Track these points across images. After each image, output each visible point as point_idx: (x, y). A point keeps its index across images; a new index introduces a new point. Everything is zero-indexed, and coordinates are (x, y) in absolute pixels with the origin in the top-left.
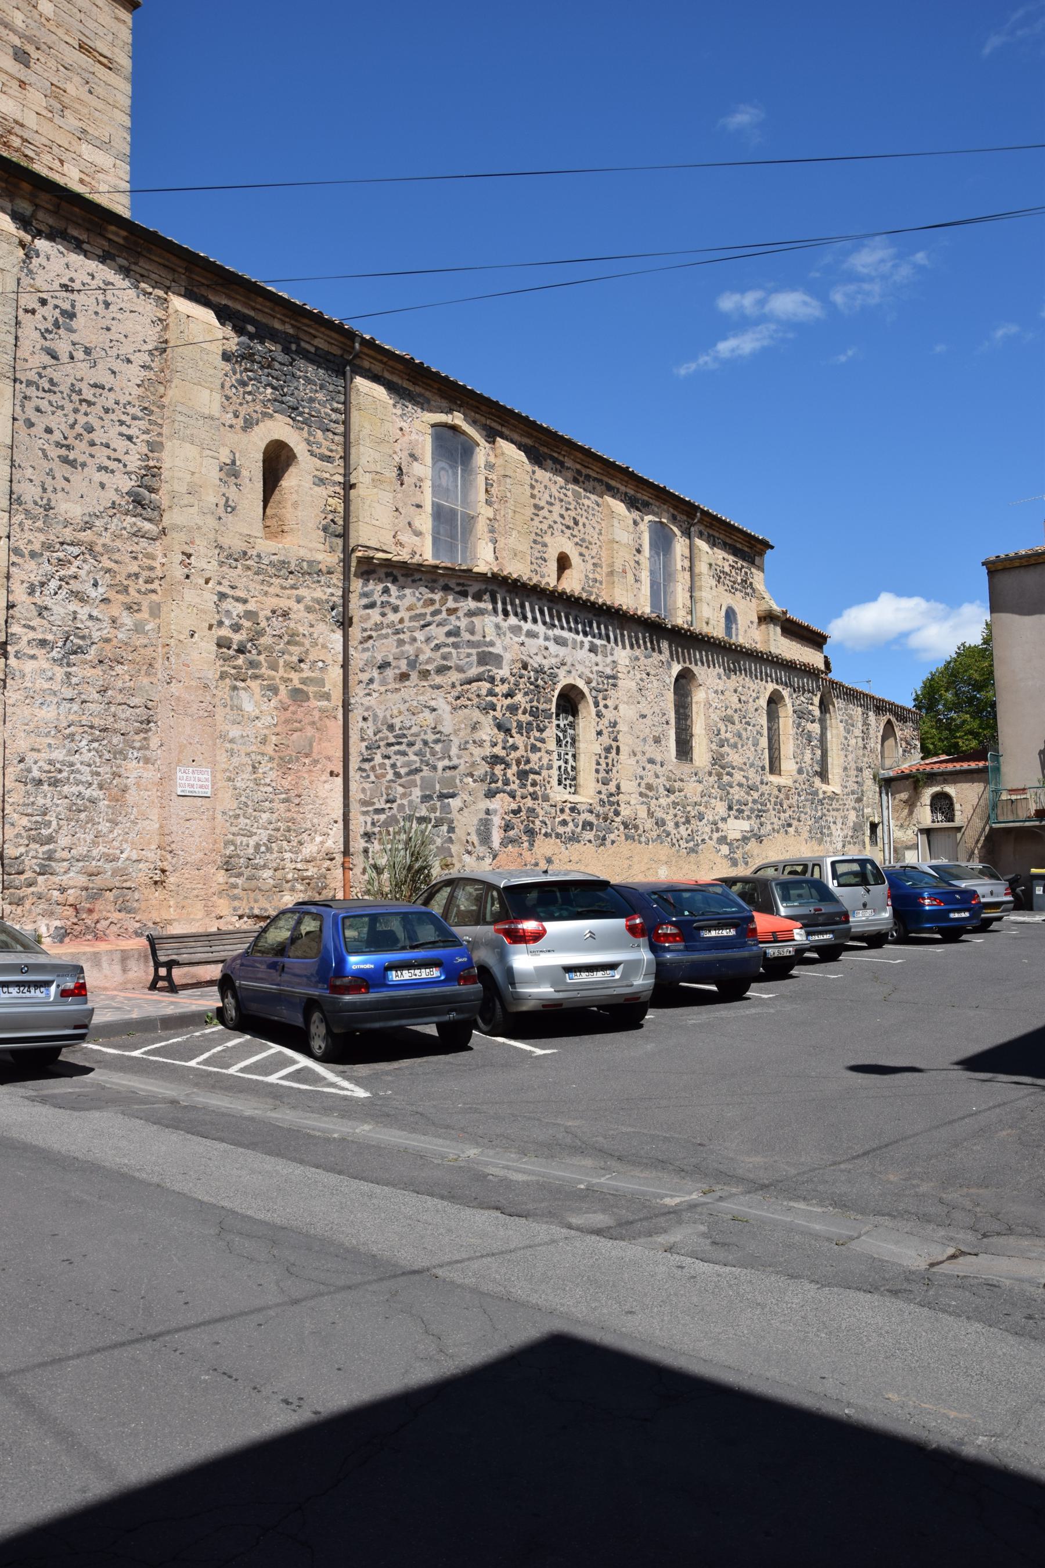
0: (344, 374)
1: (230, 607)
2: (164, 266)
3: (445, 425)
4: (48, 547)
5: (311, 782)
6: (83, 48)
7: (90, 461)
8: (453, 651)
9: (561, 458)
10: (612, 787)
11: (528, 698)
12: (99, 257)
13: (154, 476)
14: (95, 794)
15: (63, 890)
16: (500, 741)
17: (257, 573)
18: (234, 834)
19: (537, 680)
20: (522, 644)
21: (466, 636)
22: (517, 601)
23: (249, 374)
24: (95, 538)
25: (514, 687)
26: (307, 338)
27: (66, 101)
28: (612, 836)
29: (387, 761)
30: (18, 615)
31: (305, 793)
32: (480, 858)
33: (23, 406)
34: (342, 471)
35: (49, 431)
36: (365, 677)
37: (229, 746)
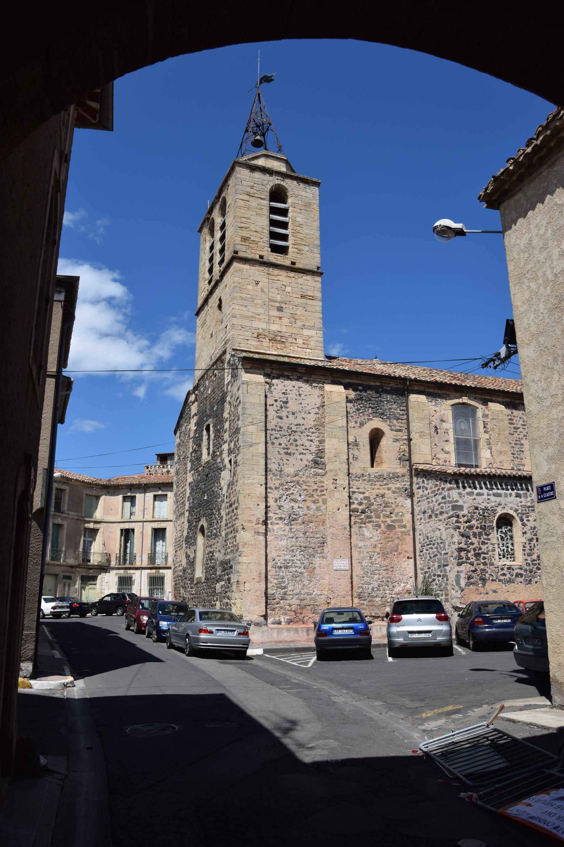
0: (405, 395)
1: (357, 496)
3: (459, 404)
4: (282, 485)
5: (398, 562)
7: (296, 452)
10: (535, 557)
11: (478, 522)
12: (296, 379)
13: (322, 452)
14: (302, 571)
15: (290, 606)
17: (369, 481)
18: (362, 584)
20: (475, 499)
22: (470, 481)
23: (361, 405)
25: (470, 518)
27: (296, 317)
28: (536, 580)
29: (427, 552)
30: (271, 510)
32: (457, 591)
34: (406, 434)
35: (280, 444)
36: (419, 517)
37: (359, 550)
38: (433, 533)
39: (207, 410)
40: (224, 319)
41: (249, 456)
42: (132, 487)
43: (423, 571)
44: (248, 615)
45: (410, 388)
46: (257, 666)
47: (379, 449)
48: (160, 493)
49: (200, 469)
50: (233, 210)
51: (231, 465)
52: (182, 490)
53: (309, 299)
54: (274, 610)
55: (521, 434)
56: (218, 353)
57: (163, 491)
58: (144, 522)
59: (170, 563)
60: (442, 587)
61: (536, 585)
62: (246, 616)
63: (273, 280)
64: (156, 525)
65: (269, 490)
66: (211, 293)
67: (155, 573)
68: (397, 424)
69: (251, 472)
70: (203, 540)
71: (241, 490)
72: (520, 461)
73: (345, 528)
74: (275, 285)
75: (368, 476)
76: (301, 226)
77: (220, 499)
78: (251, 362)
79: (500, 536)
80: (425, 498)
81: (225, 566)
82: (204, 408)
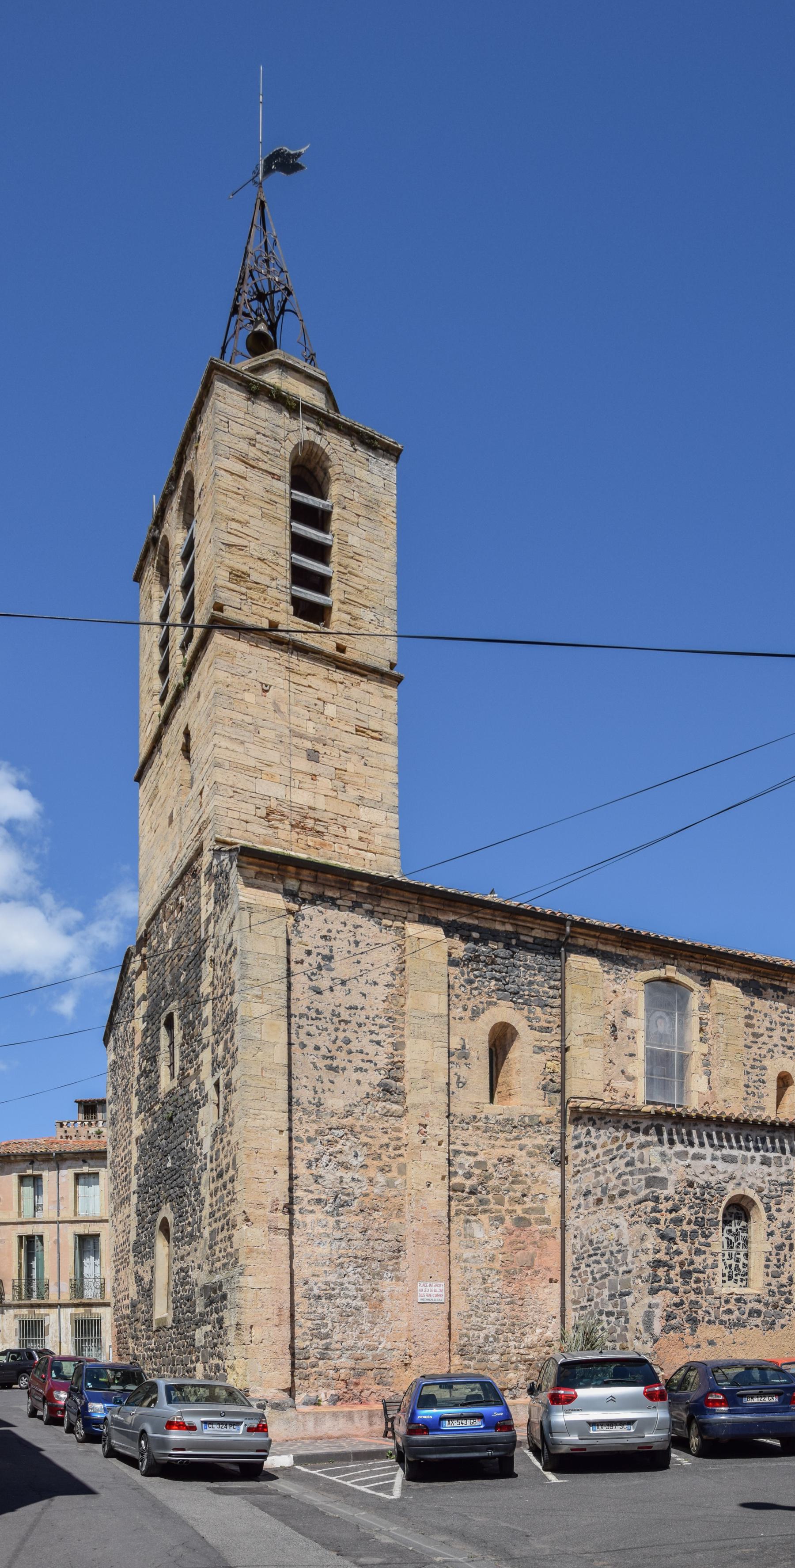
0: (559, 955)
1: (462, 1160)
2: (401, 901)
3: (660, 979)
4: (320, 1133)
5: (533, 1288)
6: (360, 731)
7: (348, 1066)
8: (630, 1178)
9: (783, 985)
10: (784, 1279)
11: (693, 1211)
13: (398, 1069)
14: (359, 1304)
16: (663, 1248)
17: (486, 1131)
18: (467, 1329)
19: (703, 1194)
20: (688, 1166)
21: (638, 1165)
22: (684, 1131)
23: (476, 972)
24: (354, 1122)
25: (679, 1203)
26: (525, 932)
28: (782, 1321)
29: (588, 1269)
30: (300, 1183)
31: (527, 1296)
32: (645, 1343)
33: (297, 1034)
34: (559, 1037)
35: (317, 1048)
36: (575, 1203)
37: (463, 1264)
38: (603, 1233)
39: (167, 984)
40: (196, 775)
41: (255, 1070)
42: (32, 1158)
43: (578, 1306)
44: (258, 1388)
45: (569, 941)
46: (290, 1496)
47: (505, 1068)
48: (86, 1169)
49: (156, 1108)
50: (210, 498)
51: (218, 1092)
52: (123, 1154)
53: (372, 738)
54: (307, 1377)
55: (764, 1046)
56: (186, 854)
57: (90, 1166)
58: (60, 1222)
59: (109, 1297)
60: (615, 1335)
61: (783, 1331)
62: (255, 1391)
63: (299, 684)
64: (81, 1229)
65: (295, 1144)
66: (166, 721)
67: (84, 1314)
68: (543, 1017)
69: (258, 1105)
70: (167, 1248)
71: (240, 1141)
72: (758, 1100)
73: (440, 1222)
74: (303, 698)
75: (485, 1121)
76: (357, 557)
77: (199, 1164)
78: (257, 861)
79: (727, 1238)
80: (590, 1165)
81: (212, 1295)
82: (161, 982)
